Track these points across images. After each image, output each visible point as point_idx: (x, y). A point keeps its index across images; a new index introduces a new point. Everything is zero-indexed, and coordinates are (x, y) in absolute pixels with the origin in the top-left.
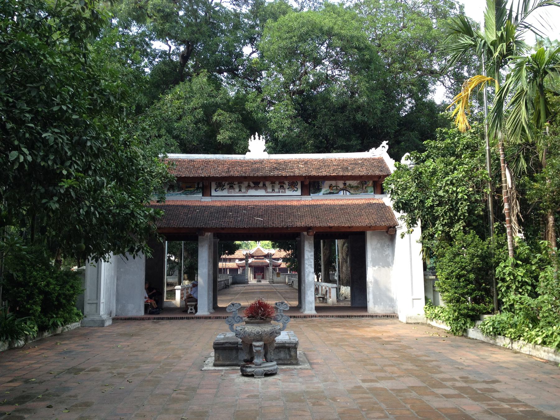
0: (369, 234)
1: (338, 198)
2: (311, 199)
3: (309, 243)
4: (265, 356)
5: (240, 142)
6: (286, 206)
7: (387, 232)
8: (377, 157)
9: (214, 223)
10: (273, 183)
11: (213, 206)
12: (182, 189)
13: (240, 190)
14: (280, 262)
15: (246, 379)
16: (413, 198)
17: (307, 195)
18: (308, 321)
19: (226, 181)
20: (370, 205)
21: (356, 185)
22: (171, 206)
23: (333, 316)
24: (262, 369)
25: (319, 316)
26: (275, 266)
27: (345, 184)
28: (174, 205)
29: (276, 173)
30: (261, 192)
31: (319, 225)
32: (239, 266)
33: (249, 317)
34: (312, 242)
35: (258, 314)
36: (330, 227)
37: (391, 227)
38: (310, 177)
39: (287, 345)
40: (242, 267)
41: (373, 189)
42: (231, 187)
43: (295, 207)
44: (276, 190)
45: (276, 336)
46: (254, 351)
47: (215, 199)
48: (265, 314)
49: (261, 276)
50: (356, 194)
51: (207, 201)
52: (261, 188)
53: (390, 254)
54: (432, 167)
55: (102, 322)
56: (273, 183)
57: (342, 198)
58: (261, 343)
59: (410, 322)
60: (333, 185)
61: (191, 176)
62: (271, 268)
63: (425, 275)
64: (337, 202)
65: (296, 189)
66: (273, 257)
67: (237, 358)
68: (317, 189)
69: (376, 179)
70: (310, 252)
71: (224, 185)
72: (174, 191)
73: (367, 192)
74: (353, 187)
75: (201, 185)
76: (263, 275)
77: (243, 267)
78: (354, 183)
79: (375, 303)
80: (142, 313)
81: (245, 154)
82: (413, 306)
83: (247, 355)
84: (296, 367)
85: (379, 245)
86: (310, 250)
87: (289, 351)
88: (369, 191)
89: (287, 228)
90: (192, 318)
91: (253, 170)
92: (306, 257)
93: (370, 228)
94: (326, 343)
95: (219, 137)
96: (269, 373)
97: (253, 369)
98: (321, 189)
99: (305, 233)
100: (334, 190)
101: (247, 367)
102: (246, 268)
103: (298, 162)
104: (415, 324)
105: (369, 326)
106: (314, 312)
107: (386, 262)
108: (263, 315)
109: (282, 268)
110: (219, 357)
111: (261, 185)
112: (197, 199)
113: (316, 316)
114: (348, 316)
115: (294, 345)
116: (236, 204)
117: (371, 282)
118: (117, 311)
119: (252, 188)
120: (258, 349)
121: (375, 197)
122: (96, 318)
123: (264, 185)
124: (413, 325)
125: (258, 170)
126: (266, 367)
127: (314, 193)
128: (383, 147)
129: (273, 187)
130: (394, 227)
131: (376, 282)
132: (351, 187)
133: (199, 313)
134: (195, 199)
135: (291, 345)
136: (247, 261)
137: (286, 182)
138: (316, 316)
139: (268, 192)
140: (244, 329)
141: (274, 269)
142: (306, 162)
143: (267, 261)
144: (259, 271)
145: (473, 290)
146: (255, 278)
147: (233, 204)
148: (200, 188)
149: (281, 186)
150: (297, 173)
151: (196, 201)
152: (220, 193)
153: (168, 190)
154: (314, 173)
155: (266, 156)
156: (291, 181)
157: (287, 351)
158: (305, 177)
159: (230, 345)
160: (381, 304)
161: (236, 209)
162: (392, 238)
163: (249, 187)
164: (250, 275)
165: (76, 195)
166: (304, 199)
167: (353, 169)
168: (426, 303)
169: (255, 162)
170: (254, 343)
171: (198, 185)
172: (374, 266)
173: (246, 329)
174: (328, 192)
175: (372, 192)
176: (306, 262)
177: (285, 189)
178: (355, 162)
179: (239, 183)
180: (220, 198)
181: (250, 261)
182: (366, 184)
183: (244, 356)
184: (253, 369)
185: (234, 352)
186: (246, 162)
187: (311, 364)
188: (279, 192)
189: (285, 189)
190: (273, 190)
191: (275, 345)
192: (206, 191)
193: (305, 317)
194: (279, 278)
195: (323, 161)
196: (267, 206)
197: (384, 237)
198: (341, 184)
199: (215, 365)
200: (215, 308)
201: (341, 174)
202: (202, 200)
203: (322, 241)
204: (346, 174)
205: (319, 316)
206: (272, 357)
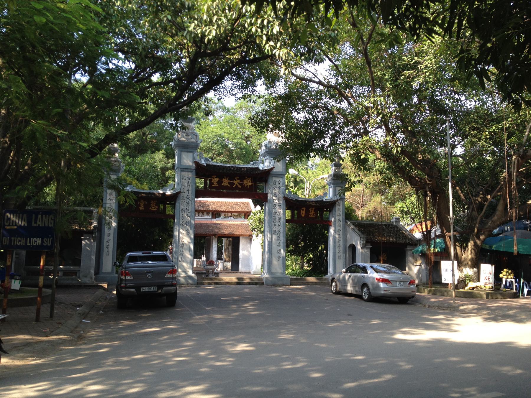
0: (241, 238)
54: (394, 106)
68: (219, 216)
78: (236, 214)
100: (226, 217)
156: (208, 212)
162: (251, 240)
165: (473, 363)
178: (237, 204)
195: (222, 203)
198: (230, 214)
201: (230, 210)
204: (233, 210)
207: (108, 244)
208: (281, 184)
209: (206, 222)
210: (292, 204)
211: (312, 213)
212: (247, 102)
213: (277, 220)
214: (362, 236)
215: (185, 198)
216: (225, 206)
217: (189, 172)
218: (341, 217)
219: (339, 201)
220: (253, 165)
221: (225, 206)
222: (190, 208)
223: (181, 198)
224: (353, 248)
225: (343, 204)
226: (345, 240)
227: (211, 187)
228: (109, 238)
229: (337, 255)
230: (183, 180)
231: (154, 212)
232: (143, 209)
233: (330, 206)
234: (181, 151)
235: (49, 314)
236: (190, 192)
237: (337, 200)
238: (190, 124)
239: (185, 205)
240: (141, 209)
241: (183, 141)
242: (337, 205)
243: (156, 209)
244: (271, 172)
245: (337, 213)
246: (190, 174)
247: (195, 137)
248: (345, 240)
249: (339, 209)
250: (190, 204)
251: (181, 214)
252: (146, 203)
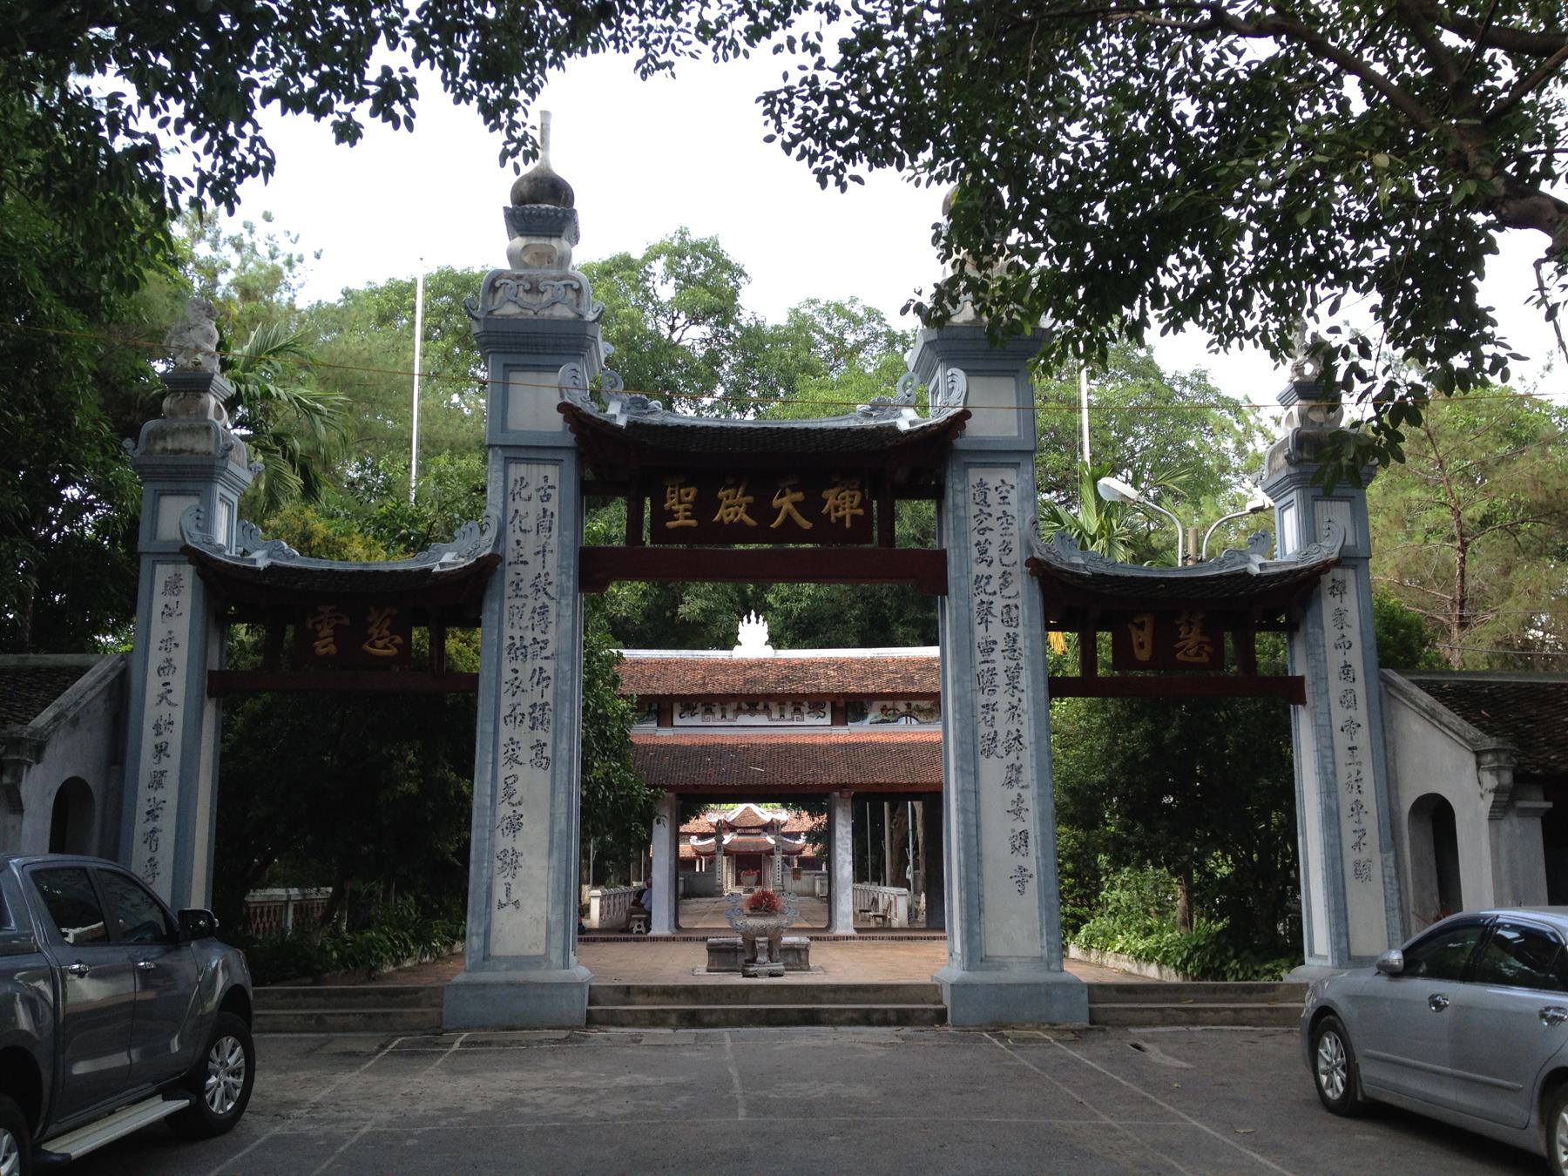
5: (720, 617)
6: (805, 745)
13: (724, 716)
14: (801, 841)
26: (789, 854)
27: (909, 705)
29: (787, 688)
30: (761, 720)
32: (698, 854)
38: (846, 695)
40: (705, 854)
44: (788, 716)
49: (752, 879)
51: (665, 735)
52: (760, 712)
62: (778, 858)
66: (784, 830)
68: (860, 715)
75: (655, 707)
76: (759, 875)
77: (711, 857)
89: (805, 785)
91: (746, 681)
92: (838, 835)
95: (682, 609)
99: (837, 794)
100: (889, 716)
102: (719, 857)
103: (827, 664)
106: (852, 932)
109: (806, 859)
111: (761, 707)
123: (766, 707)
125: (755, 681)
127: (854, 721)
132: (921, 711)
133: (654, 933)
136: (720, 840)
141: (787, 861)
142: (840, 665)
143: (770, 840)
144: (749, 863)
145: (1073, 887)
146: (738, 882)
147: (711, 741)
150: (824, 686)
152: (688, 721)
154: (853, 688)
155: (768, 653)
156: (814, 702)
163: (739, 711)
164: (726, 874)
167: (921, 680)
176: (838, 844)
180: (688, 731)
181: (728, 839)
183: (741, 959)
192: (664, 719)
193: (836, 939)
194: (798, 883)
195: (872, 662)
198: (902, 706)
200: (678, 927)
201: (901, 689)
203: (886, 805)
207: (150, 826)
208: (1013, 496)
209: (808, 741)
210: (1068, 596)
211: (1190, 642)
212: (777, 49)
213: (1002, 679)
214: (1490, 743)
215: (526, 589)
216: (880, 674)
217: (539, 461)
218: (1355, 657)
219: (1337, 573)
220: (867, 415)
221: (880, 674)
222: (551, 635)
223: (509, 591)
224: (1436, 816)
225: (1365, 587)
226: (1389, 781)
227: (659, 532)
228: (159, 795)
229: (1350, 857)
230: (520, 505)
231: (384, 663)
232: (332, 649)
233: (1290, 597)
234: (509, 368)
235: (258, 1078)
236: (552, 560)
237: (1326, 566)
238: (554, 242)
239: (526, 622)
240: (321, 651)
241: (507, 319)
242: (1326, 593)
243: (393, 651)
244: (959, 443)
245: (1331, 634)
246: (552, 472)
247: (571, 295)
248: (1389, 781)
249: (1340, 614)
250: (552, 616)
251: (507, 666)
252: (346, 621)
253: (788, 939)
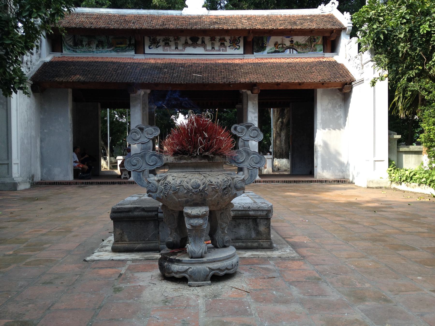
0: (319, 92)
1: (284, 57)
2: (254, 57)
3: (253, 103)
4: (212, 234)
6: (228, 64)
7: (341, 90)
8: (326, 14)
9: (146, 79)
10: (213, 39)
11: (146, 63)
12: (113, 46)
13: (177, 48)
15: (170, 288)
16: (405, 21)
17: (250, 54)
18: (253, 186)
19: (160, 35)
20: (321, 63)
21: (304, 42)
22: (100, 62)
23: (278, 182)
24: (205, 267)
25: (264, 181)
27: (292, 41)
28: (102, 62)
30: (200, 50)
31: (265, 81)
33: (175, 153)
34: (257, 102)
35: (195, 147)
36: (278, 84)
37: (346, 84)
39: (251, 213)
41: (322, 47)
42: (167, 44)
43: (237, 65)
44: (217, 48)
45: (235, 196)
46: (188, 226)
47: (148, 56)
48: (211, 146)
50: (304, 53)
53: (342, 116)
55: (14, 186)
56: (213, 39)
57: (288, 57)
58: (203, 210)
59: (371, 186)
60: (279, 43)
61: (121, 27)
63: (389, 134)
64: (283, 60)
65: (238, 47)
67: (156, 236)
68: (262, 48)
69: (327, 35)
70: (254, 113)
71: (159, 42)
72: (103, 47)
73: (316, 50)
74: (300, 45)
78: (301, 39)
79: (323, 168)
80: (71, 178)
81: (182, 9)
82: (374, 169)
83: (174, 234)
84: (269, 253)
85: (330, 106)
86: (253, 111)
87: (256, 225)
88: (318, 49)
89: (229, 84)
90: (125, 183)
93: (323, 84)
94: (291, 209)
96: (222, 273)
97: (186, 267)
98: (266, 47)
100: (279, 49)
101: (172, 261)
103: (242, 17)
104: (377, 188)
105: (328, 190)
107: (339, 124)
108: (207, 149)
110: (122, 234)
111: (199, 42)
112: (129, 57)
113: (260, 182)
114: (295, 182)
115: (265, 213)
116: (172, 62)
117: (320, 146)
118: (42, 175)
119: (190, 45)
120: (195, 222)
121: (325, 56)
122: (7, 180)
123: (203, 42)
124: (375, 190)
126: (214, 261)
127: (258, 51)
128: (333, 3)
129: (213, 44)
130: (350, 84)
131: (326, 145)
134: (127, 57)
135: (259, 213)
137: (227, 38)
138: (260, 182)
139: (207, 51)
140: (165, 178)
142: (249, 18)
147: (168, 61)
148: (133, 44)
149: (221, 44)
150: (240, 27)
151: (128, 58)
152: (154, 51)
153: (97, 46)
157: (251, 223)
158: (249, 30)
159: (143, 213)
160: (330, 169)
161: (172, 67)
163: (186, 44)
166: (247, 57)
168: (390, 164)
169: (193, 18)
170: (188, 210)
171: (130, 41)
172: (324, 128)
173: (170, 179)
174: (273, 50)
175: (321, 50)
177: (225, 47)
178: (303, 18)
179: (175, 40)
180: (155, 56)
182: (314, 41)
183: (169, 235)
184: (186, 267)
185: (152, 226)
186: (183, 18)
187: (294, 246)
188: (219, 50)
189: (226, 47)
190: (213, 48)
191: (232, 214)
196: (206, 64)
197: (336, 97)
199: (115, 250)
202: (135, 57)
205: (264, 181)
206: (227, 238)
253: (242, 201)
